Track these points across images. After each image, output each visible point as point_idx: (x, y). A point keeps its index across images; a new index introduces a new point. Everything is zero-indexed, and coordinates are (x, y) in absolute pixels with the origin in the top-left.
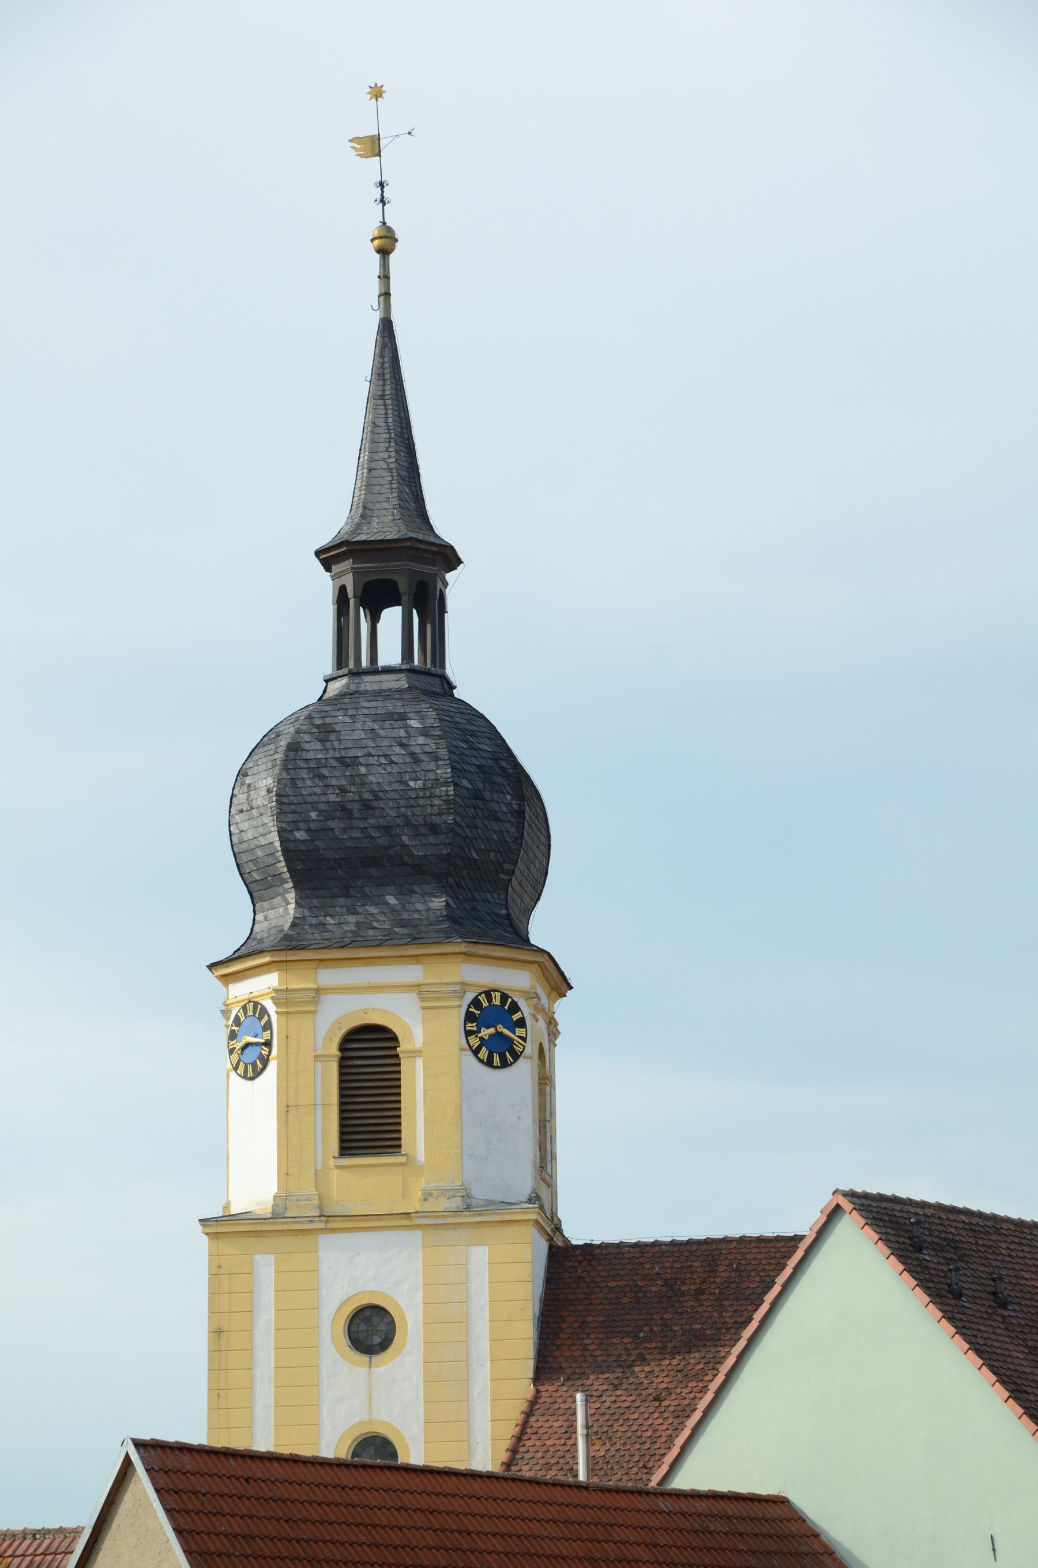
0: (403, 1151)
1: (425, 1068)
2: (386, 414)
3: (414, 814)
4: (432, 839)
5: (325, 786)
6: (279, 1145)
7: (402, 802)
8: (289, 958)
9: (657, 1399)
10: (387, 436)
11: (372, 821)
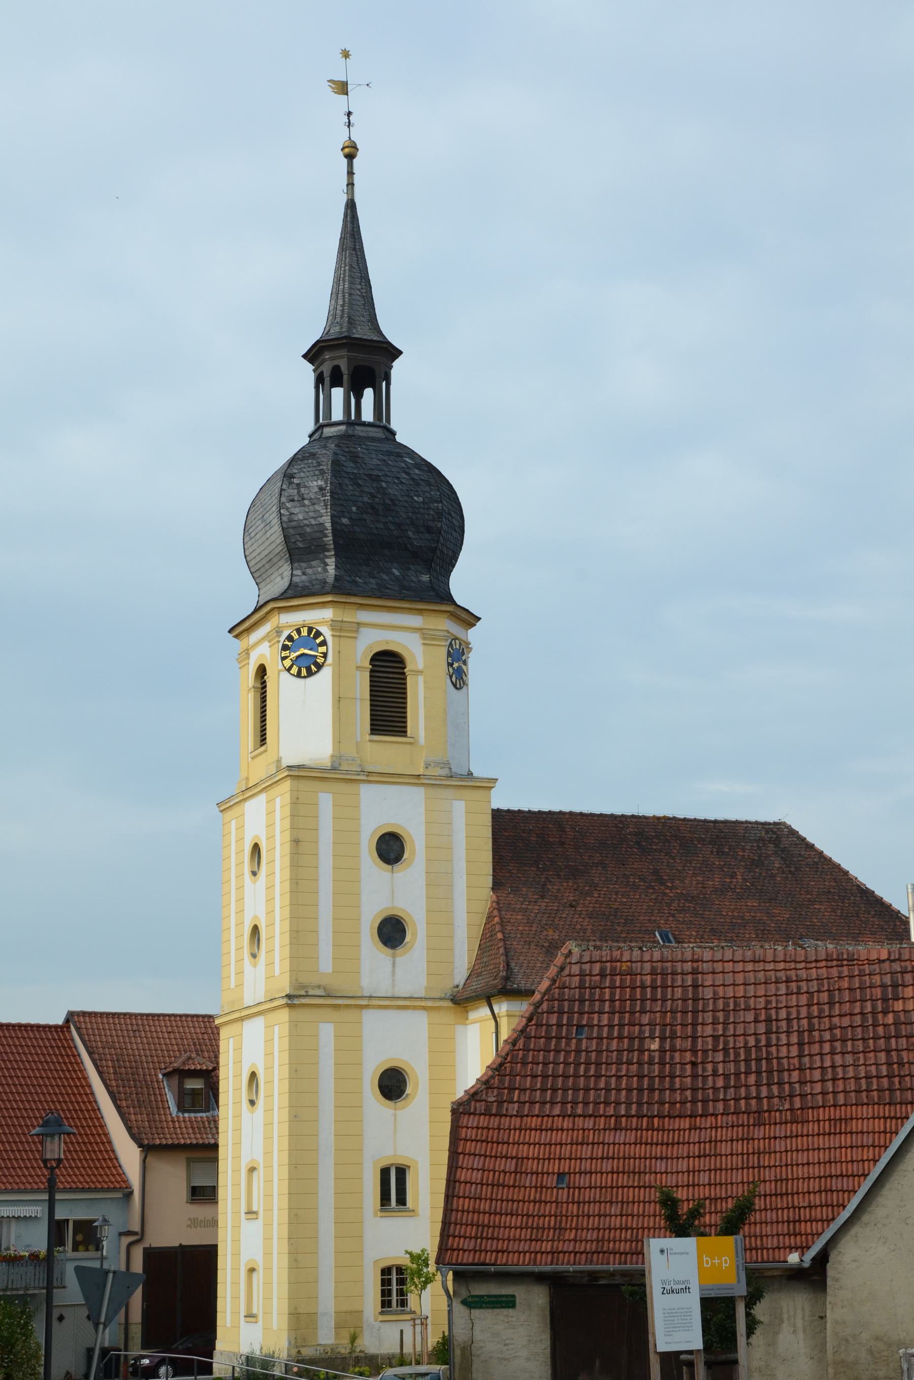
0: (409, 733)
1: (425, 682)
2: (358, 260)
3: (417, 518)
4: (427, 536)
5: (361, 491)
6: (334, 723)
7: (410, 509)
8: (347, 601)
9: (571, 906)
10: (359, 275)
11: (391, 519)
